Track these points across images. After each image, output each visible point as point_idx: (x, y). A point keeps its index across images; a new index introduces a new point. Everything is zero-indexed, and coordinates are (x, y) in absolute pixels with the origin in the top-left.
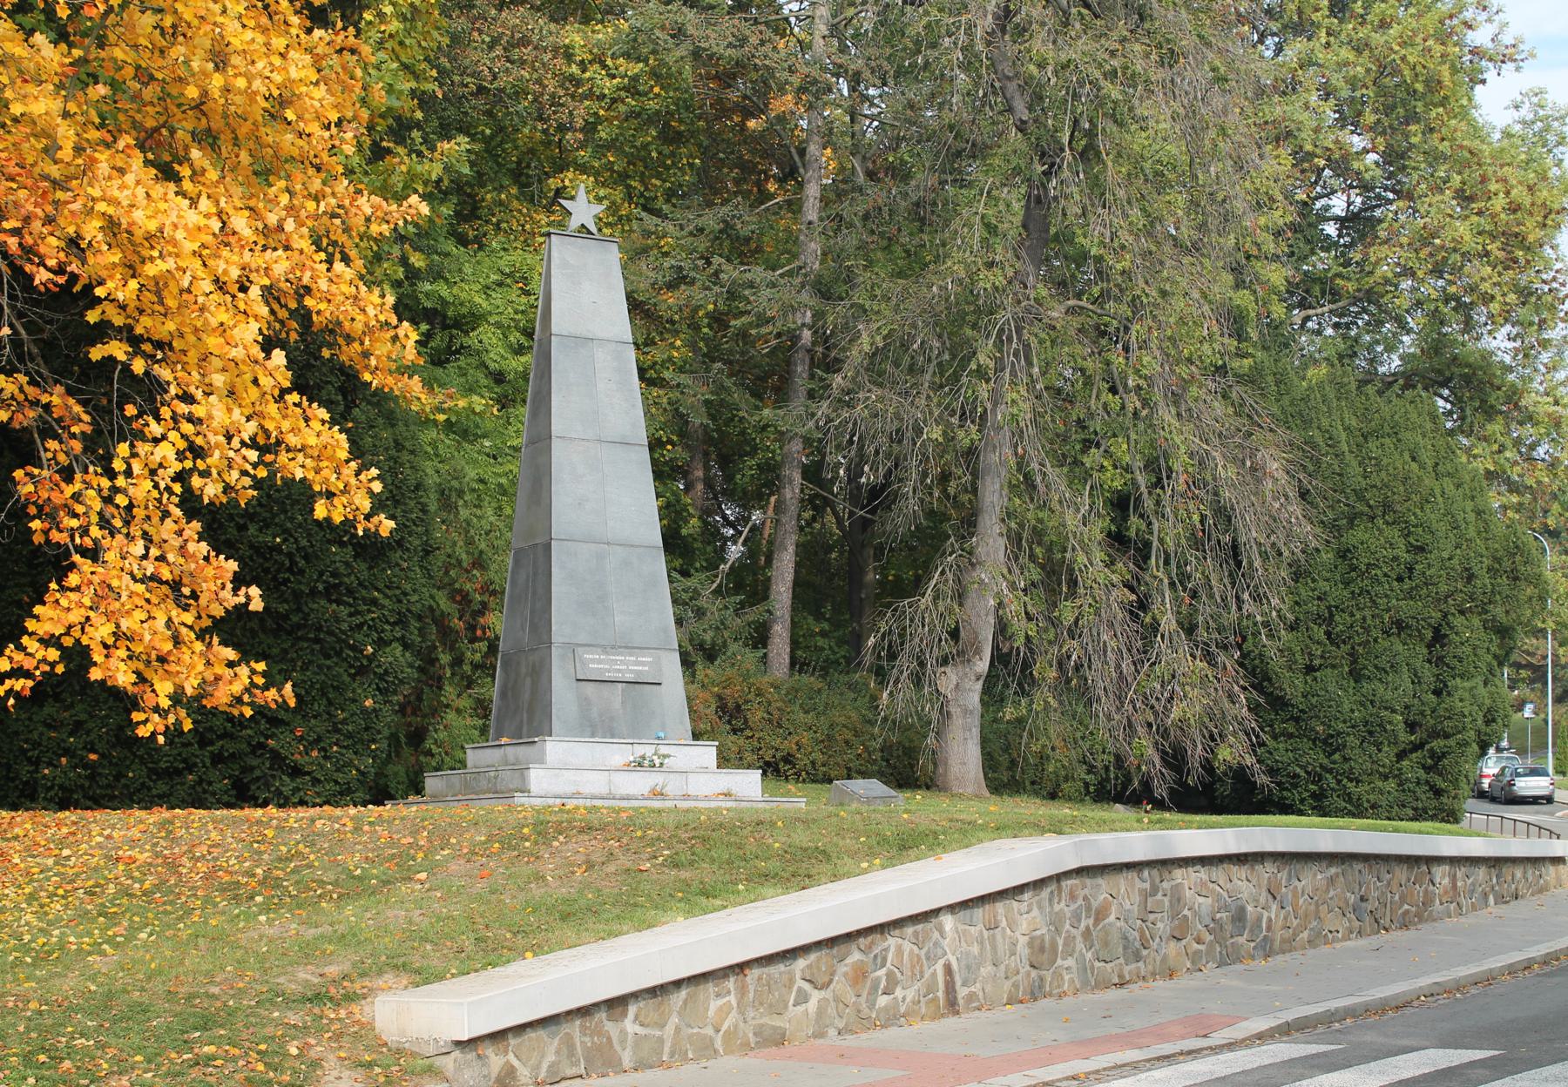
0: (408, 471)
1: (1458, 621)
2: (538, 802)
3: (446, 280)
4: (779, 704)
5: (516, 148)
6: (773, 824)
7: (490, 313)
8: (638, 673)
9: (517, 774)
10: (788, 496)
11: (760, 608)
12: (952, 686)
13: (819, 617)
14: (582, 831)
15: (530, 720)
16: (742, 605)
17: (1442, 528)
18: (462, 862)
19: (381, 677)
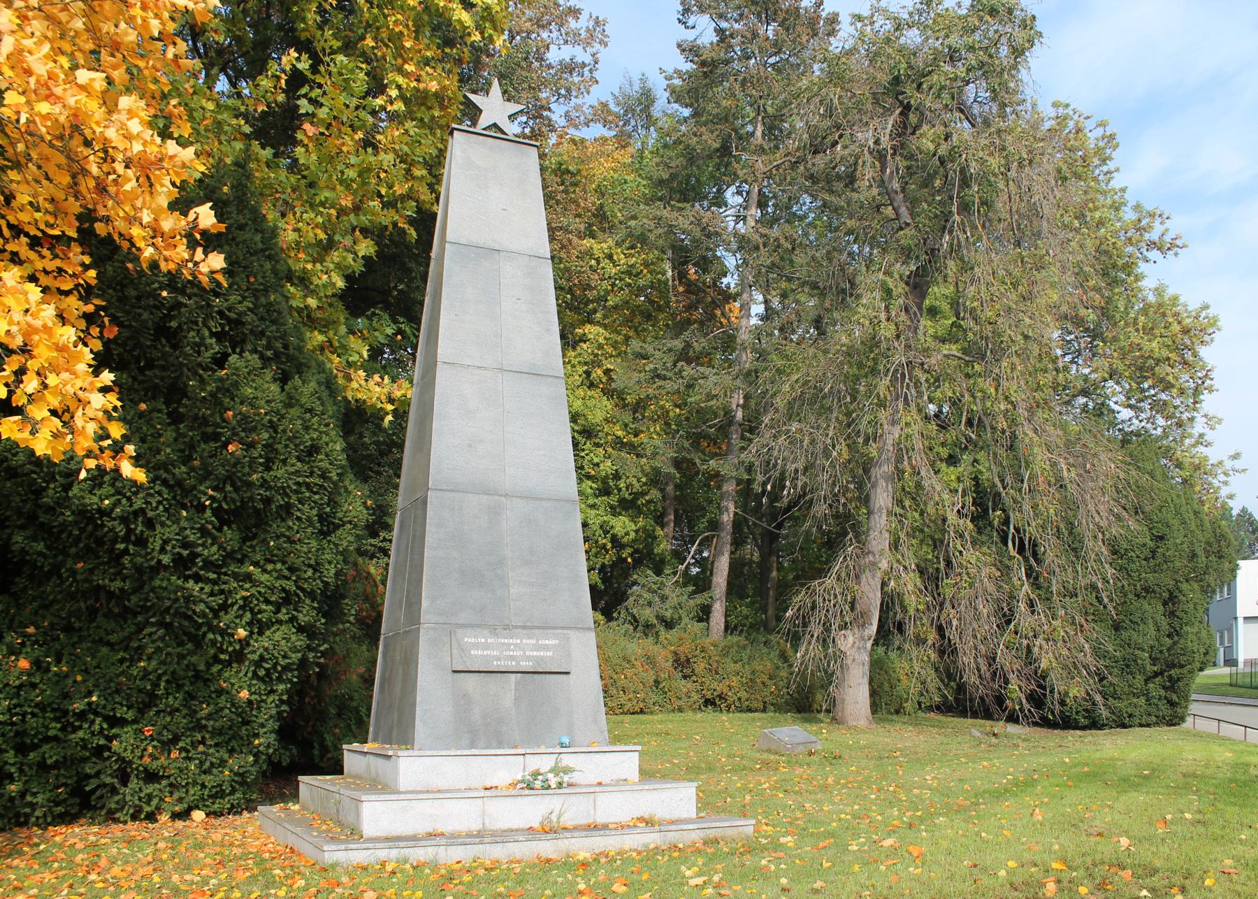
1: (1184, 586)
8: (538, 660)
11: (706, 594)
12: (849, 645)
16: (694, 592)
17: (1175, 523)
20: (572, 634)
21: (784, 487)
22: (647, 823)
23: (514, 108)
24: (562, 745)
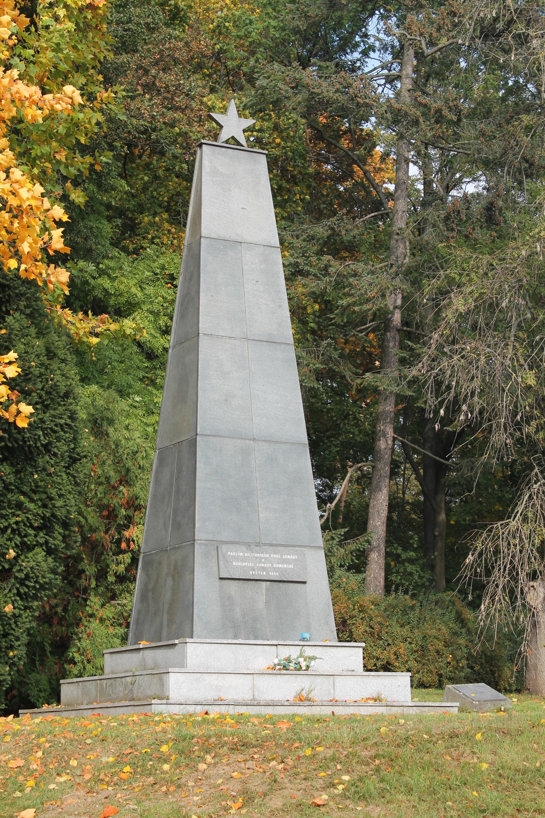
0: (58, 378)
2: (175, 709)
3: (109, 276)
4: (379, 619)
5: (168, 191)
6: (469, 737)
7: (144, 302)
9: (156, 679)
10: (383, 447)
11: (361, 539)
13: (406, 547)
14: (234, 749)
15: (171, 622)
16: (347, 536)
18: (82, 793)
19: (22, 582)
20: (306, 551)
21: (459, 410)
22: (375, 700)
24: (303, 639)
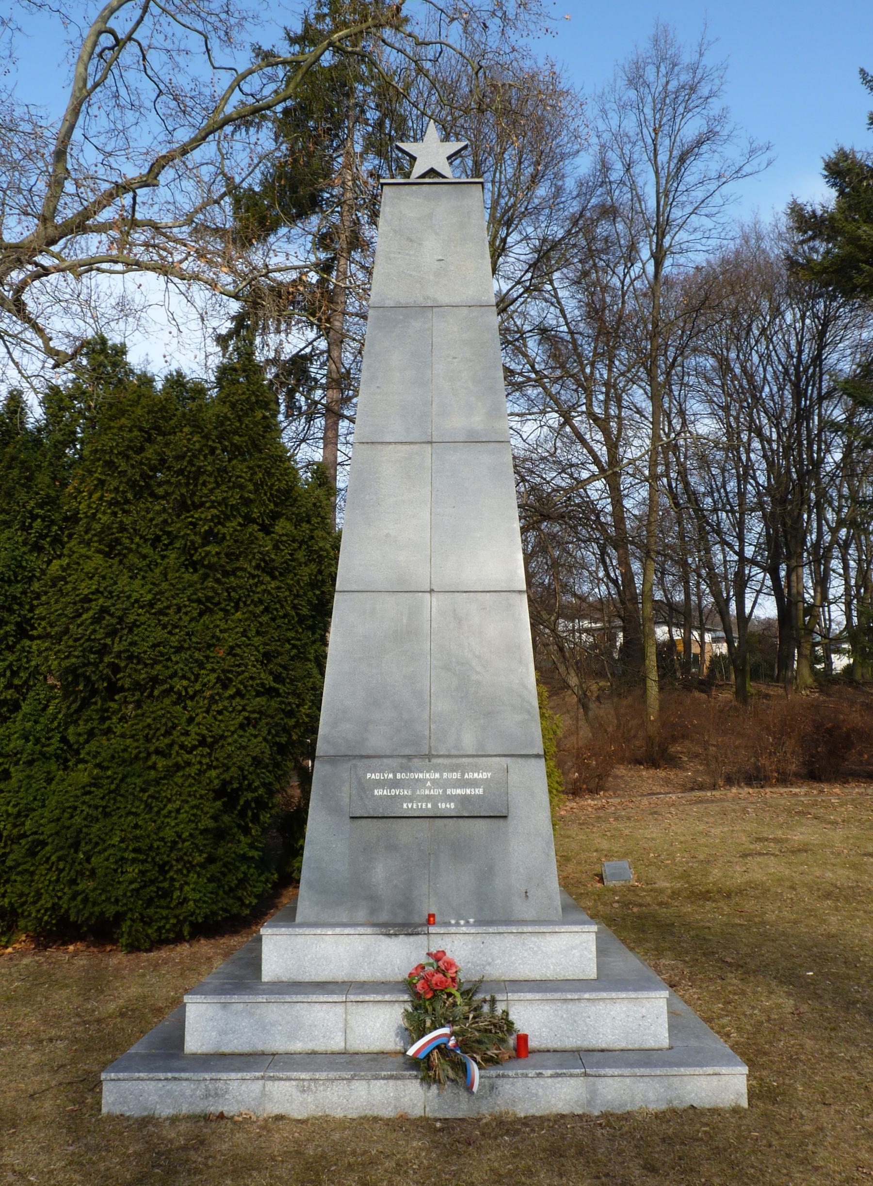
23: (454, 146)
